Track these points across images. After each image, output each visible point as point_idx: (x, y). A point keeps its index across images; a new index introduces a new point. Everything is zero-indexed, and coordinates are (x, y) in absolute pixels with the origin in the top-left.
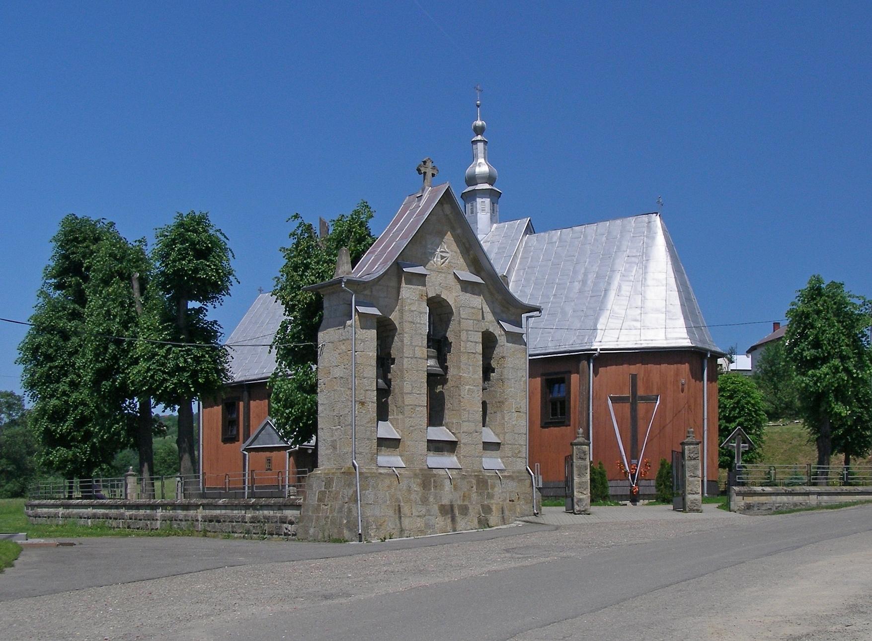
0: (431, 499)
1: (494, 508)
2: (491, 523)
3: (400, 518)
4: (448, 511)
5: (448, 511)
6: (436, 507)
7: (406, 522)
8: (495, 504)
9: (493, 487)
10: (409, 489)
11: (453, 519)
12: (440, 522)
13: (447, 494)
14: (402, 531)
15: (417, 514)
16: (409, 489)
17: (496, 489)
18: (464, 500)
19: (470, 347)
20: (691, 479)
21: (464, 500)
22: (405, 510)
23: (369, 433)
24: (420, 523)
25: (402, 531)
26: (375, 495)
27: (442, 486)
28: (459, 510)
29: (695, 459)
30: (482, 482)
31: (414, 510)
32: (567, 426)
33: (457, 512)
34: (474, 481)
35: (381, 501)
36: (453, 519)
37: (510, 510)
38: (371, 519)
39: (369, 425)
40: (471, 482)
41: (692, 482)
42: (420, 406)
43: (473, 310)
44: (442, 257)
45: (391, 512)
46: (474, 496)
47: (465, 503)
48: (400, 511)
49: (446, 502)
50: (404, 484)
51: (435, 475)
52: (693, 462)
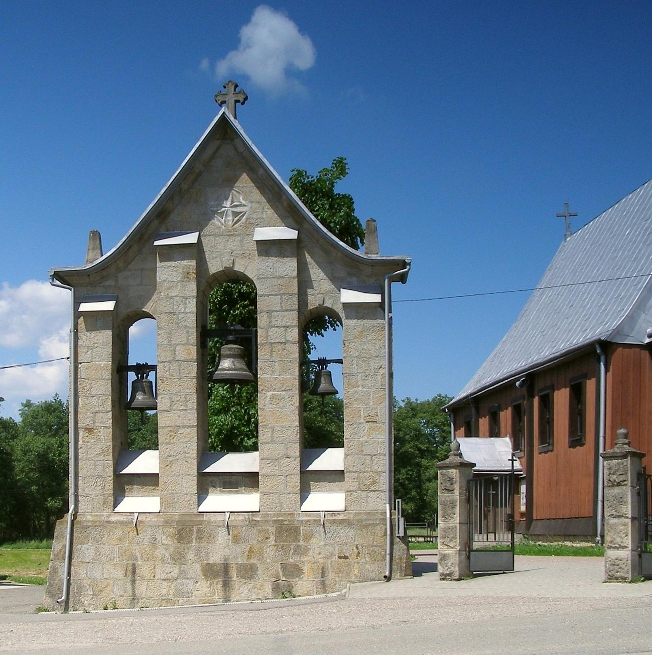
0: (191, 555)
1: (306, 568)
2: (297, 590)
3: (133, 581)
4: (221, 574)
5: (221, 574)
6: (198, 567)
7: (141, 588)
8: (307, 563)
9: (308, 537)
10: (154, 541)
11: (226, 584)
12: (203, 588)
13: (220, 549)
14: (134, 599)
15: (164, 576)
16: (154, 541)
17: (313, 541)
18: (249, 557)
19: (275, 335)
20: (613, 521)
21: (249, 557)
22: (144, 570)
23: (100, 468)
24: (165, 589)
25: (134, 599)
26: (97, 549)
27: (211, 538)
28: (239, 571)
29: (619, 484)
30: (288, 531)
31: (158, 571)
32: (247, 450)
33: (234, 573)
34: (272, 529)
35: (104, 559)
36: (226, 584)
37: (338, 572)
38: (86, 582)
39: (101, 458)
40: (267, 531)
41: (613, 527)
42: (184, 427)
43: (280, 281)
44: (235, 214)
45: (120, 574)
46: (270, 552)
47: (253, 561)
48: (134, 572)
49: (216, 558)
50: (145, 536)
51: (201, 523)
52: (617, 490)
